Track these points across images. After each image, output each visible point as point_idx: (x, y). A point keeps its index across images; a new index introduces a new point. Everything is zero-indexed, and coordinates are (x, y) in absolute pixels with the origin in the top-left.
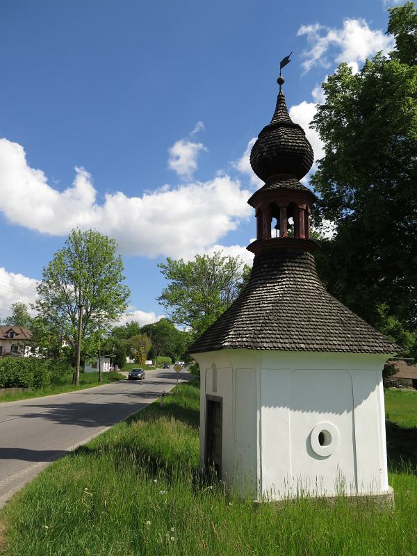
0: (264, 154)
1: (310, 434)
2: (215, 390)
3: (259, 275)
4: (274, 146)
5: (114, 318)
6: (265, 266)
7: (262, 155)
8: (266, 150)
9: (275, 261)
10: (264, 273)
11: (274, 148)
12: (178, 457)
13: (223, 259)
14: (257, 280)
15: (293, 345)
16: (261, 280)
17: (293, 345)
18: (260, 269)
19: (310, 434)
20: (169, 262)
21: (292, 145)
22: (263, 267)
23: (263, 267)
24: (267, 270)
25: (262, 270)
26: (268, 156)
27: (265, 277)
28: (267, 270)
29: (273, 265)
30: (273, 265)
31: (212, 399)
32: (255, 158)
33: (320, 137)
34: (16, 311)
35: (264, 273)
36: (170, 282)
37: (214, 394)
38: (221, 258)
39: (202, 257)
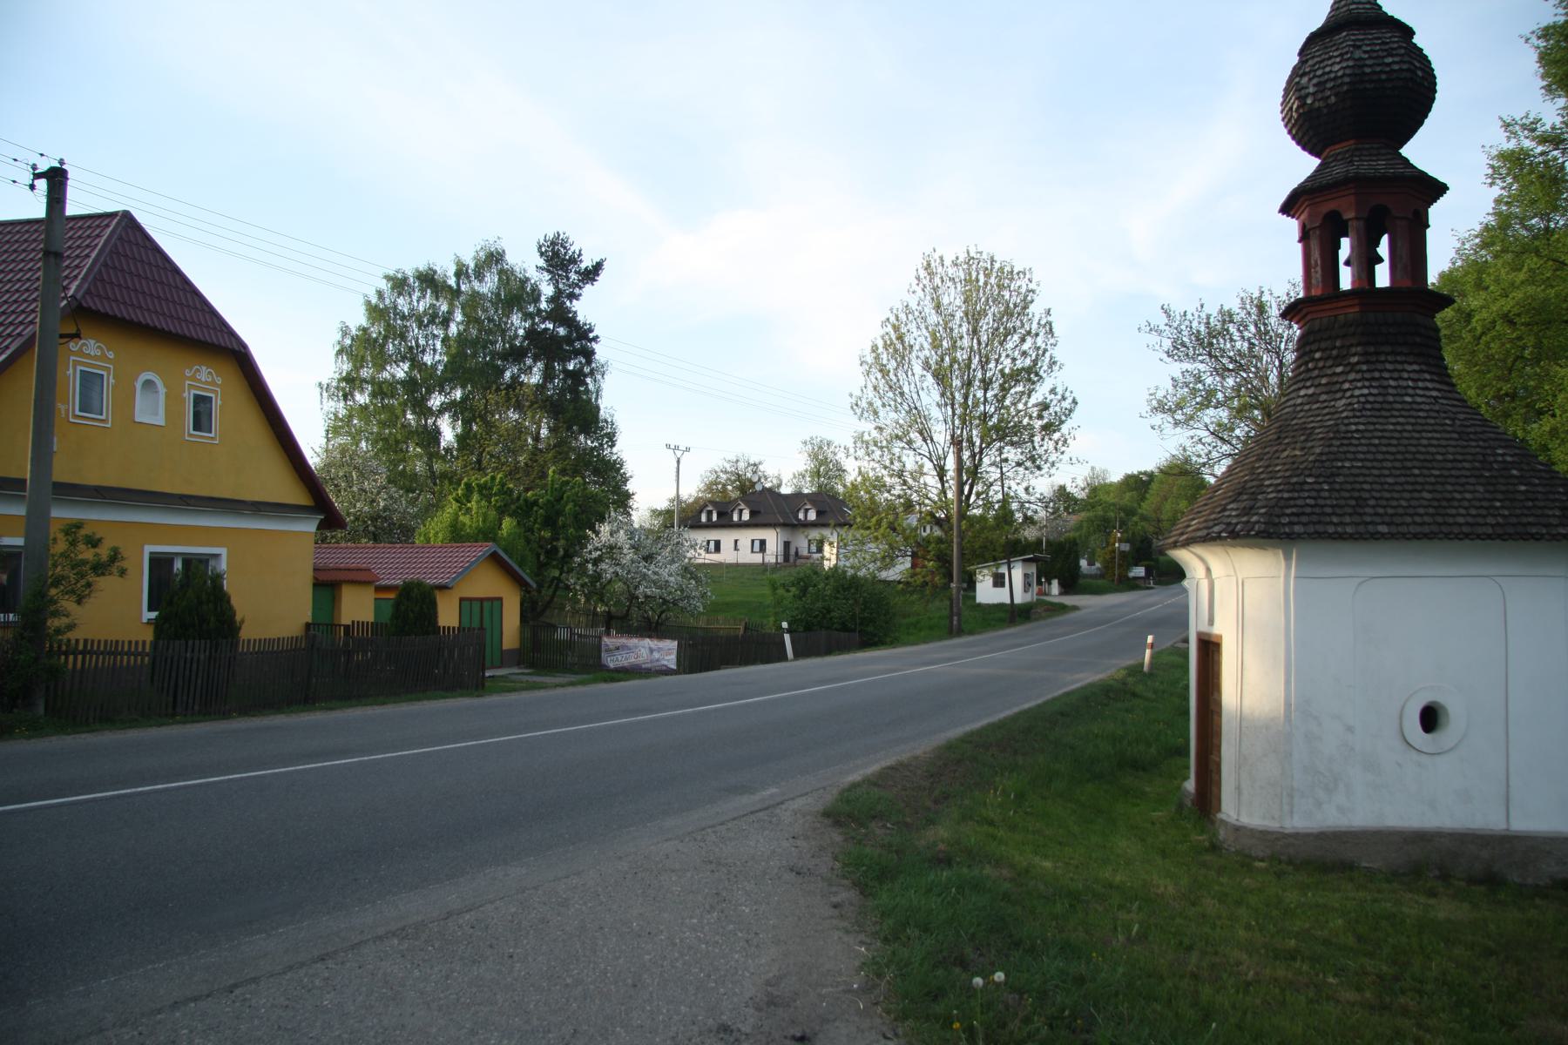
1: (1403, 708)
2: (1211, 622)
4: (1331, 80)
5: (1039, 468)
6: (1317, 355)
8: (1311, 90)
9: (1338, 344)
10: (1316, 372)
11: (1329, 85)
12: (818, 474)
14: (1300, 389)
15: (1361, 529)
16: (1307, 388)
17: (1361, 529)
19: (1403, 708)
20: (1169, 316)
21: (1374, 73)
22: (1313, 359)
23: (1313, 359)
24: (1321, 364)
25: (1310, 365)
26: (1317, 104)
27: (1316, 382)
28: (1321, 364)
29: (1335, 352)
30: (1335, 352)
31: (1206, 638)
32: (1291, 108)
34: (814, 456)
35: (1316, 372)
36: (1176, 368)
39: (1257, 294)
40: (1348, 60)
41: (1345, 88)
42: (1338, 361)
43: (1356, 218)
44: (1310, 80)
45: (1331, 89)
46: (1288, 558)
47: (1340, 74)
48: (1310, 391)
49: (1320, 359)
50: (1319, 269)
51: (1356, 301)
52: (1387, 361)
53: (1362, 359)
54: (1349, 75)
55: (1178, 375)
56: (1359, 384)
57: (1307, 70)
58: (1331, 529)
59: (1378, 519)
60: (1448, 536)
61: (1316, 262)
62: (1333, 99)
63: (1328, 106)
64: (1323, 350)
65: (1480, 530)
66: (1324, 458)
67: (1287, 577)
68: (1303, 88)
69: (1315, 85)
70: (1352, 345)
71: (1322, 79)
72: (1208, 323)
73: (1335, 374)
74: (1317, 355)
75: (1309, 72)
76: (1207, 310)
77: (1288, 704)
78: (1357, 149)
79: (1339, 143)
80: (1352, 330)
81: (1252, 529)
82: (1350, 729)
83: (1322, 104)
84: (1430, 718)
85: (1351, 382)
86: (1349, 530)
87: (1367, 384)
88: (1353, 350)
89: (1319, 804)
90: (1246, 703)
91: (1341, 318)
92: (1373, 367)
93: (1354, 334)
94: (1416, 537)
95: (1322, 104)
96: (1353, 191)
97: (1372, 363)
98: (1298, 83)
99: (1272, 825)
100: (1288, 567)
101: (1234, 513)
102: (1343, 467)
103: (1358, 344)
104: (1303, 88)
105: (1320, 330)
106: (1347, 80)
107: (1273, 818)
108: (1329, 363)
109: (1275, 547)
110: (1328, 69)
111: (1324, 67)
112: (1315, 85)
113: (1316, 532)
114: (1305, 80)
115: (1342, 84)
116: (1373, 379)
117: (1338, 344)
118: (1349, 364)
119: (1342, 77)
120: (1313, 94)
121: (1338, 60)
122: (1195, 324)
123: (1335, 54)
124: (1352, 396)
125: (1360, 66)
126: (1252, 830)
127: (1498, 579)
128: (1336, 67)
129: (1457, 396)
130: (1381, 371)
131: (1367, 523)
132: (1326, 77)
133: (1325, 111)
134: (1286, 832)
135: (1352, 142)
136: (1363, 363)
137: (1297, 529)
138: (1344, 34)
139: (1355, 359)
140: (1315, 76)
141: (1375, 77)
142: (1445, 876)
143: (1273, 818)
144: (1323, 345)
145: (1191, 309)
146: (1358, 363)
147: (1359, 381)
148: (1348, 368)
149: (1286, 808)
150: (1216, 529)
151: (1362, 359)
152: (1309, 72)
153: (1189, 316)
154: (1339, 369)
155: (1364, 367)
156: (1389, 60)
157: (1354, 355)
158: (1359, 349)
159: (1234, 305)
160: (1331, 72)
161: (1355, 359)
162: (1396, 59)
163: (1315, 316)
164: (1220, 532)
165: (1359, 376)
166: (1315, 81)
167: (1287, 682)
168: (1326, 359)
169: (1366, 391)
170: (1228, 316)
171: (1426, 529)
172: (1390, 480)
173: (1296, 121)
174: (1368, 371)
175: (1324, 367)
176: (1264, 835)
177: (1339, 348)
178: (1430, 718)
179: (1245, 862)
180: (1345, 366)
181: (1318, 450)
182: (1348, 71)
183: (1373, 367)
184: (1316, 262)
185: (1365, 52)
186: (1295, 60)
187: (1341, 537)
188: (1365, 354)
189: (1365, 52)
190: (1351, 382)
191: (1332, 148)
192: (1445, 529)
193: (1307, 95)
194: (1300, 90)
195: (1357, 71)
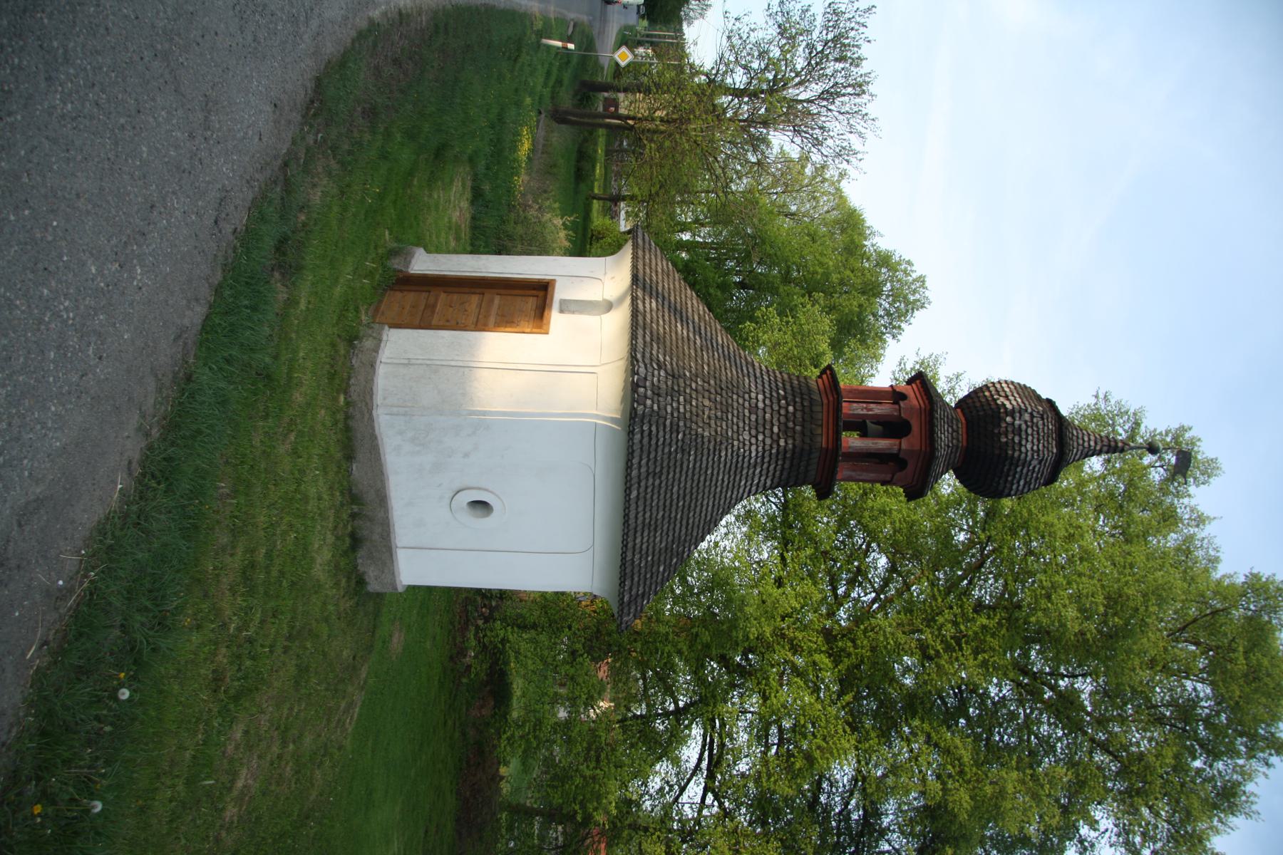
0: (1008, 419)
1: (486, 490)
2: (566, 307)
3: (774, 394)
6: (791, 409)
7: (1007, 413)
8: (1017, 422)
9: (798, 428)
13: (860, 135)
16: (764, 401)
18: (785, 398)
19: (486, 490)
21: (1016, 472)
22: (788, 404)
23: (788, 404)
24: (783, 412)
25: (783, 402)
26: (1003, 425)
27: (768, 410)
28: (783, 412)
29: (791, 425)
30: (791, 425)
33: (1208, 530)
37: (556, 305)
38: (863, 131)
40: (1033, 455)
41: (1010, 452)
42: (785, 430)
43: (900, 449)
44: (1026, 422)
45: (1013, 439)
46: (613, 420)
47: (1023, 449)
48: (761, 405)
49: (787, 411)
50: (865, 412)
51: (830, 446)
52: (777, 465)
53: (781, 449)
54: (1020, 456)
55: (813, 10)
56: (760, 449)
57: (1035, 420)
58: (635, 461)
59: (642, 490)
60: (625, 535)
61: (871, 410)
62: (1004, 440)
63: (1000, 433)
64: (794, 414)
65: (629, 554)
66: (699, 440)
67: (597, 416)
68: (1021, 415)
69: (1020, 425)
70: (794, 440)
71: (1023, 433)
72: (853, 46)
73: (772, 425)
74: (791, 409)
75: (1032, 421)
76: (865, 46)
77: (484, 413)
78: (957, 447)
79: (967, 434)
80: (808, 440)
81: (639, 404)
82: (466, 455)
83: (1003, 429)
84: (481, 506)
85: (763, 441)
86: (634, 473)
87: (760, 454)
88: (790, 441)
89: (401, 433)
90: (485, 373)
91: (819, 431)
92: (773, 457)
93: (803, 441)
94: (626, 516)
95: (1003, 429)
96: (923, 449)
97: (777, 456)
98: (1026, 410)
99: (379, 398)
100: (605, 419)
101: (655, 379)
102: (690, 455)
103: (794, 445)
104: (1021, 415)
105: (812, 411)
106: (1016, 454)
107: (385, 399)
108: (783, 419)
109: (623, 412)
110: (1030, 438)
111: (1032, 435)
112: (1020, 425)
113: (633, 451)
114: (1027, 417)
115: (1014, 450)
116: (763, 457)
117: (798, 428)
118: (779, 438)
119: (1020, 450)
120: (1013, 424)
121: (1035, 448)
122: (852, 34)
123: (1041, 446)
124: (751, 444)
125: (1025, 463)
126: (372, 380)
127: (591, 550)
128: (1029, 446)
129: (745, 495)
130: (769, 462)
131: (639, 484)
132: (1024, 437)
133: (996, 431)
134: (374, 412)
135: (965, 444)
136: (778, 450)
137: (638, 437)
138: (1055, 451)
139: (782, 443)
140: (1027, 426)
141: (1011, 473)
142: (353, 516)
143: (385, 399)
144: (799, 415)
145: (868, 33)
146: (778, 445)
147: (763, 448)
148: (775, 437)
149: (395, 410)
150: (642, 370)
151: (781, 449)
152: (1032, 421)
153: (862, 29)
154: (776, 429)
155: (774, 451)
156: (1022, 483)
157: (786, 442)
158: (790, 446)
159: (865, 67)
160: (1027, 441)
161: (782, 443)
162: (1021, 488)
163: (825, 407)
164: (638, 374)
165: (767, 447)
166: (1024, 427)
167: (504, 414)
168: (786, 416)
169: (753, 454)
170: (857, 62)
171: (632, 521)
172: (675, 489)
173: (995, 400)
174: (771, 454)
175: (780, 415)
176: (368, 393)
177: (794, 429)
178: (481, 506)
179: (352, 339)
180: (778, 434)
181: (706, 434)
182: (1023, 456)
183: (773, 457)
184: (871, 410)
185: (1034, 467)
186: (1044, 397)
187: (628, 467)
188: (785, 451)
189: (1034, 467)
190: (763, 441)
191: (964, 426)
192: (631, 533)
193: (1014, 418)
194: (1020, 412)
195: (1020, 463)
